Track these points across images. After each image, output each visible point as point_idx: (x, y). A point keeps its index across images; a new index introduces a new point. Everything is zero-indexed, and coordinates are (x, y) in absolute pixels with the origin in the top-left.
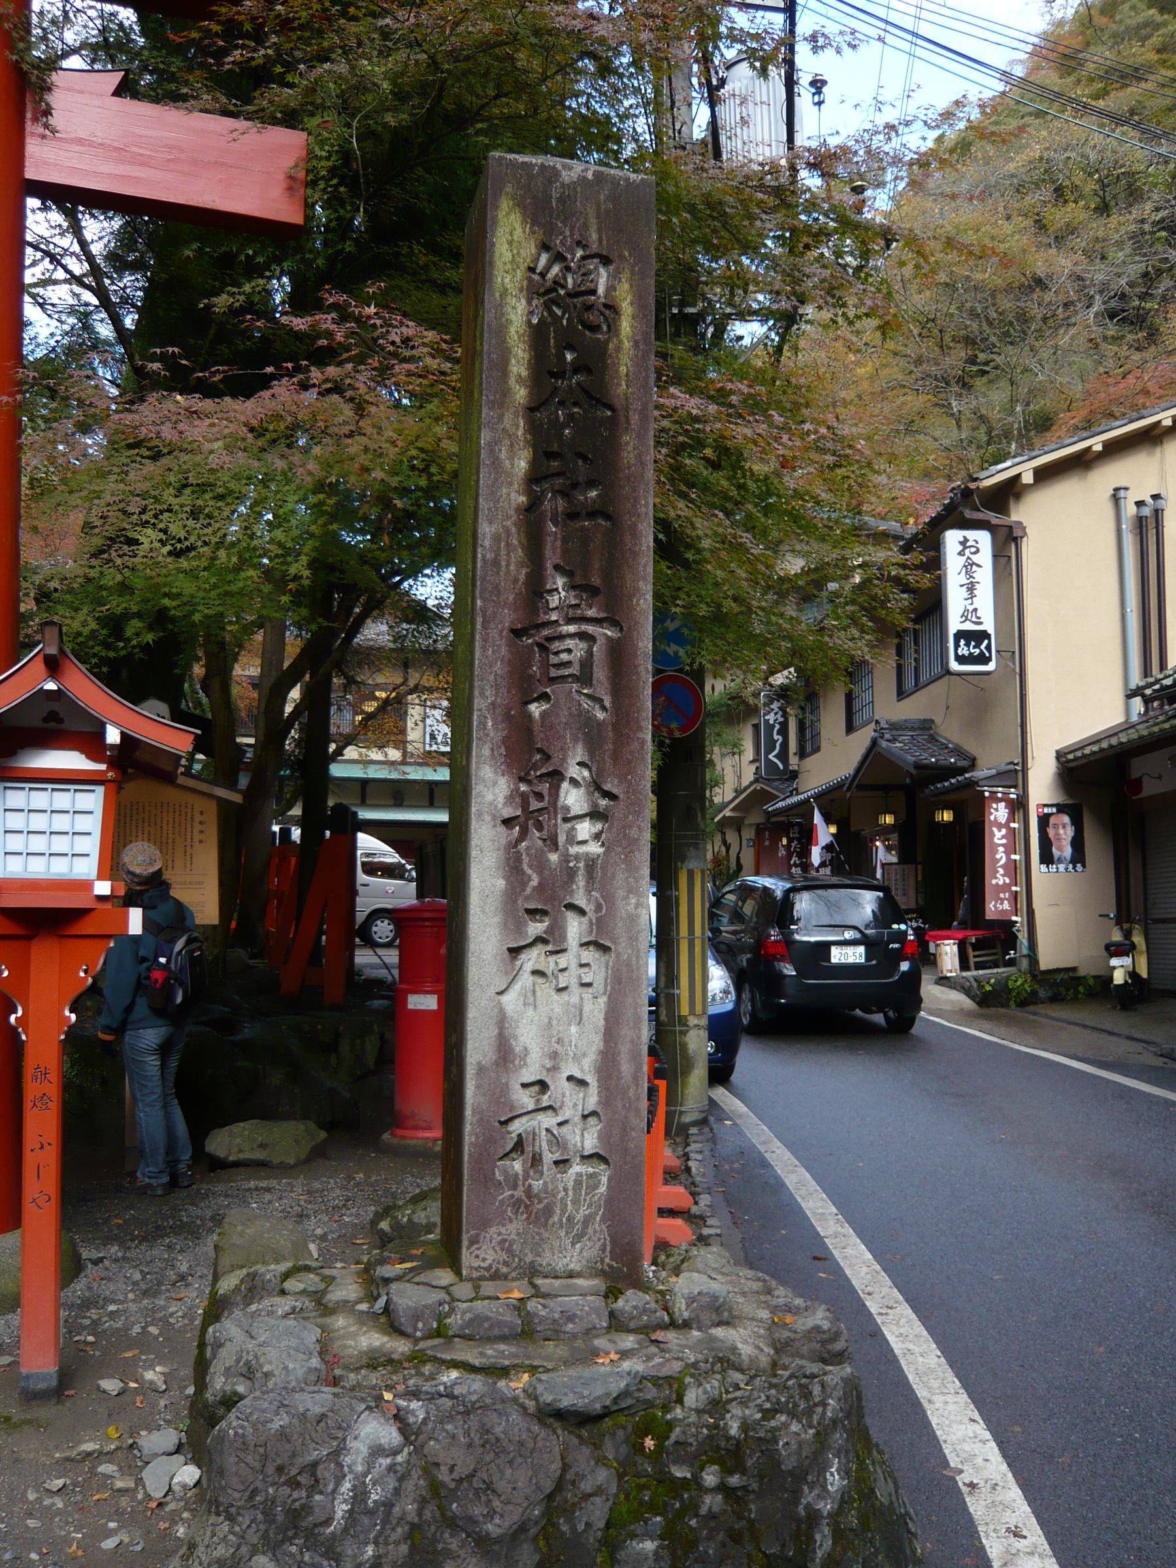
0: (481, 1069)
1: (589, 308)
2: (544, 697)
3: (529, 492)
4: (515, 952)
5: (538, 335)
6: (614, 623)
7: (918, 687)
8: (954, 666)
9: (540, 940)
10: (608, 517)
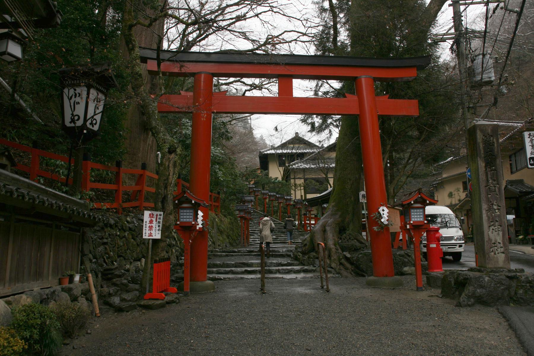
0: (487, 241)
1: (490, 143)
2: (490, 194)
3: (485, 168)
4: (489, 226)
5: (484, 148)
6: (498, 184)
7: (517, 170)
8: (530, 166)
9: (493, 225)
10: (496, 170)
